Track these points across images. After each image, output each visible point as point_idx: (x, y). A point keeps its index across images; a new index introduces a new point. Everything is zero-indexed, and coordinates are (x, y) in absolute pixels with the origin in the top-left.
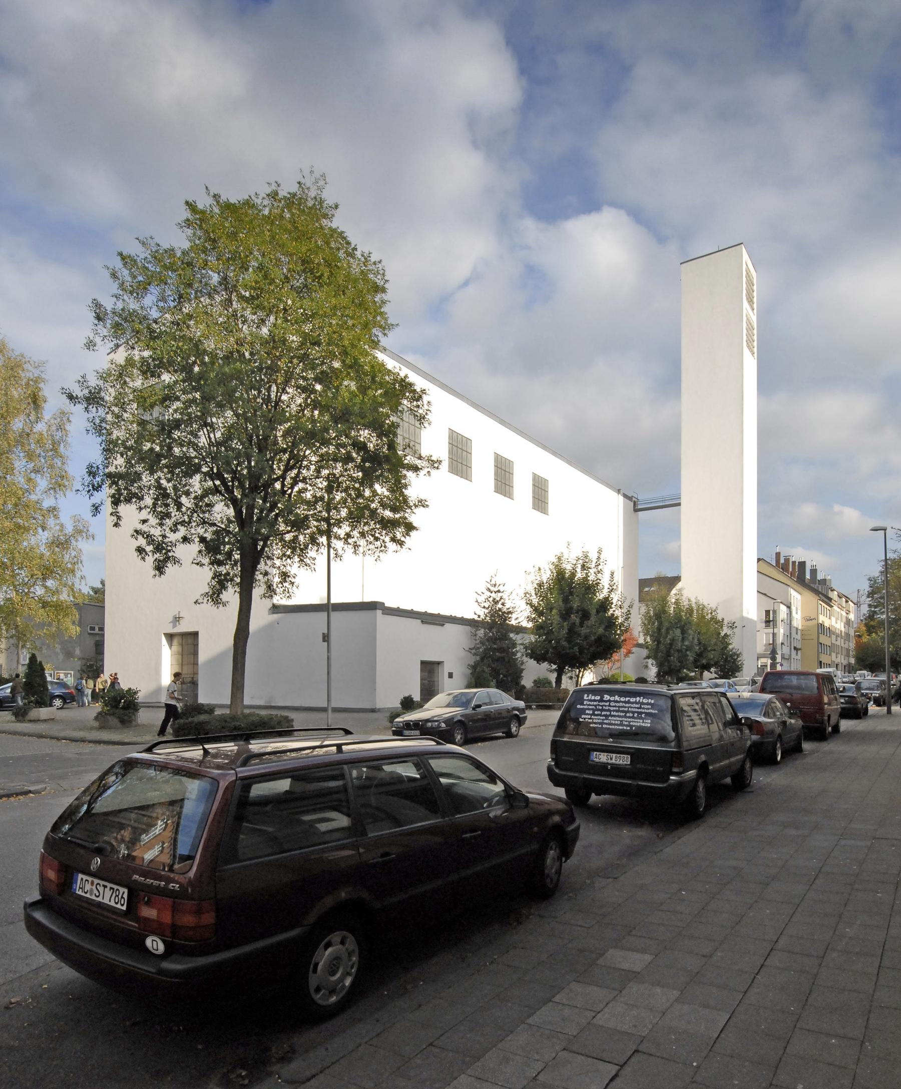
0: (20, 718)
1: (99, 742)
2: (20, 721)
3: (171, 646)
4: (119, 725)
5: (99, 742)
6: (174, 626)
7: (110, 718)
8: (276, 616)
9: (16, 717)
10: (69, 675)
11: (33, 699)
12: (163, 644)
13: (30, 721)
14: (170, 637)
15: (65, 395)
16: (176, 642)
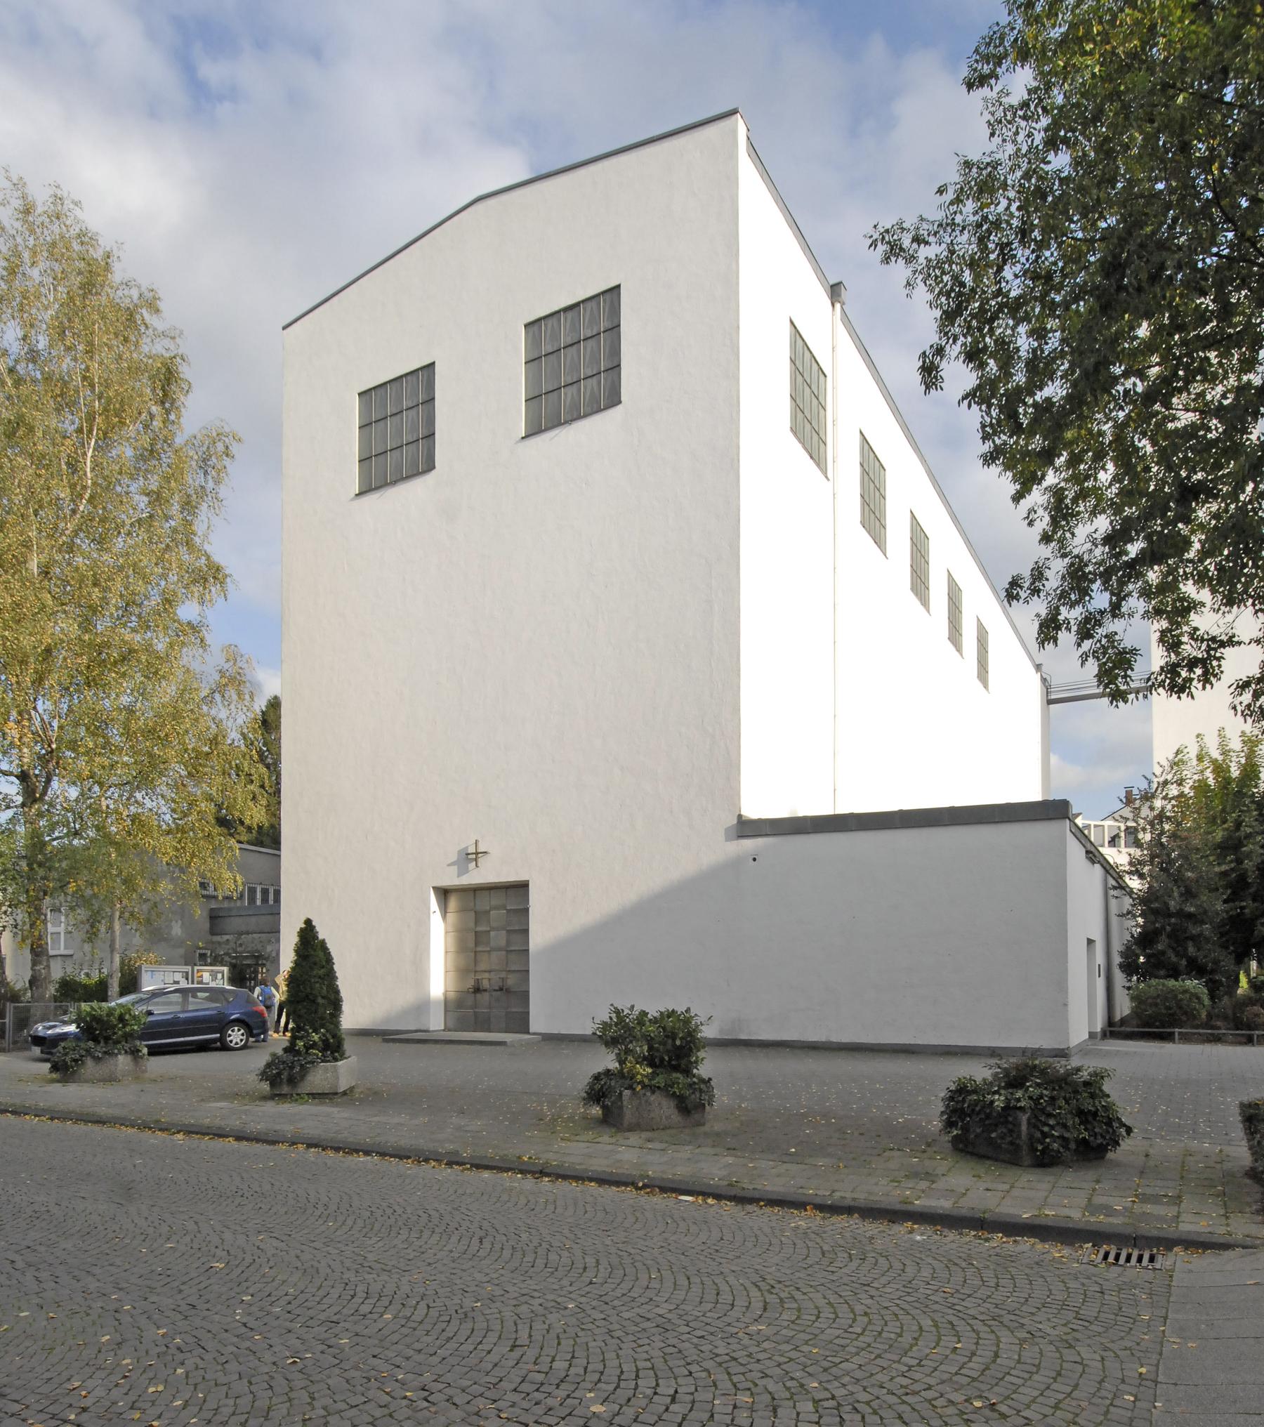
0: (285, 1089)
1: (982, 1224)
2: (282, 1097)
3: (444, 912)
4: (676, 1117)
5: (982, 1224)
6: (463, 871)
7: (655, 1098)
8: (749, 844)
9: (272, 1085)
10: (220, 976)
11: (316, 1037)
12: (432, 910)
13: (314, 1096)
14: (444, 894)
15: (957, 159)
16: (453, 903)
